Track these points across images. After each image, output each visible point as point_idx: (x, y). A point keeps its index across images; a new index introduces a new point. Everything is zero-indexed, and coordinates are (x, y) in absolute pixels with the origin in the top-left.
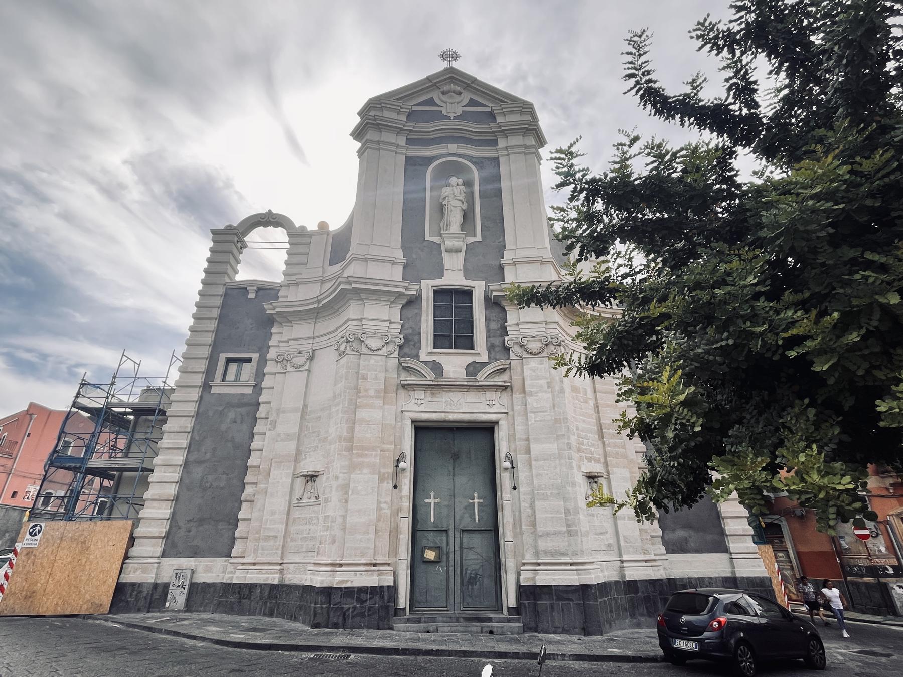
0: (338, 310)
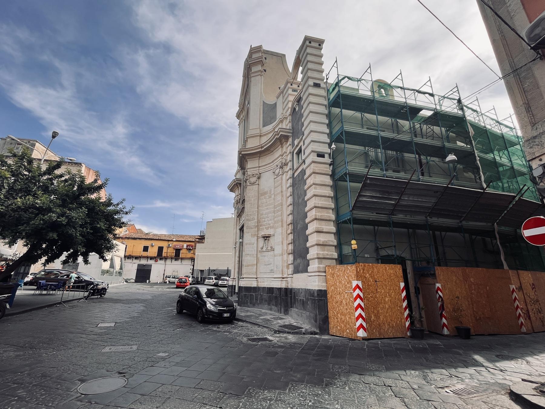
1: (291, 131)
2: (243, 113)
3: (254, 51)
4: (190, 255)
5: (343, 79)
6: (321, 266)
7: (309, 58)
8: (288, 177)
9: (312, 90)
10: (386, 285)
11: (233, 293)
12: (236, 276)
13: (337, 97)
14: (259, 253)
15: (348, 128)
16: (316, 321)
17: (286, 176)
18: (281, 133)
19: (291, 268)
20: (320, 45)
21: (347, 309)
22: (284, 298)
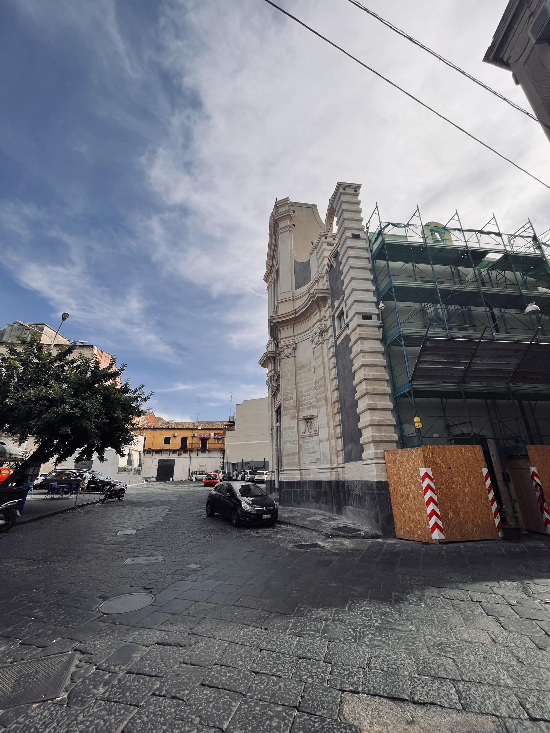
0: (309, 316)
1: (330, 291)
2: (272, 274)
3: (279, 204)
4: (218, 445)
6: (379, 451)
9: (350, 243)
10: (463, 472)
12: (275, 468)
15: (397, 282)
16: (377, 521)
17: (327, 344)
18: (317, 295)
20: (356, 191)
21: (415, 505)
22: (336, 494)
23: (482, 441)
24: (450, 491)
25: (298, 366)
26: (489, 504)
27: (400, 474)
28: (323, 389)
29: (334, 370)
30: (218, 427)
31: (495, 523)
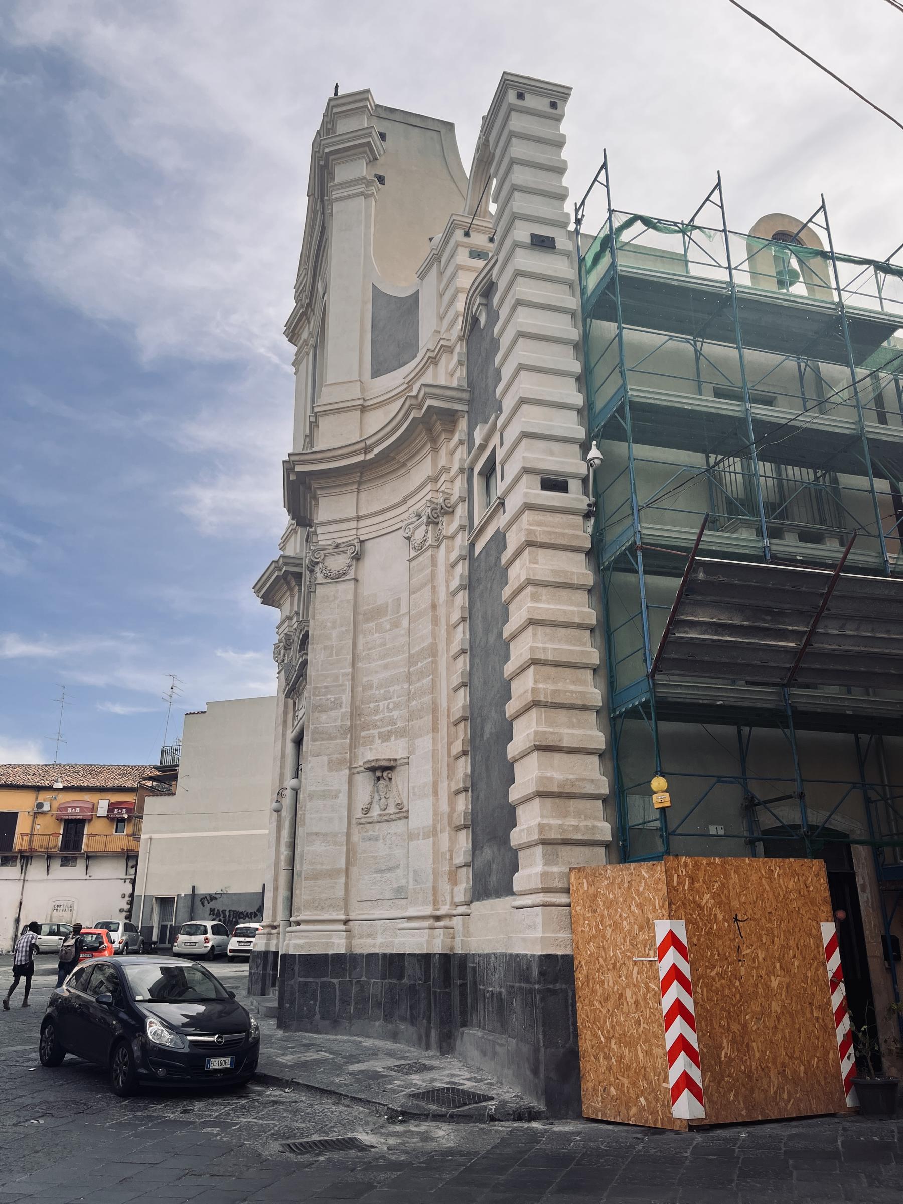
0: (404, 464)
1: (465, 396)
2: (308, 321)
3: (343, 107)
4: (120, 842)
5: (628, 224)
6: (555, 869)
7: (518, 149)
8: (454, 556)
9: (527, 260)
10: (770, 932)
11: (269, 982)
12: (281, 915)
13: (607, 288)
14: (355, 830)
15: (641, 391)
16: (535, 1071)
17: (449, 550)
18: (429, 402)
19: (465, 878)
20: (554, 105)
21: (638, 1023)
22: (436, 992)
23: (831, 848)
24: (731, 984)
25: (364, 608)
26: (830, 1022)
27: (604, 937)
28: (427, 681)
29: (460, 628)
30: (121, 782)
31: (839, 1072)
